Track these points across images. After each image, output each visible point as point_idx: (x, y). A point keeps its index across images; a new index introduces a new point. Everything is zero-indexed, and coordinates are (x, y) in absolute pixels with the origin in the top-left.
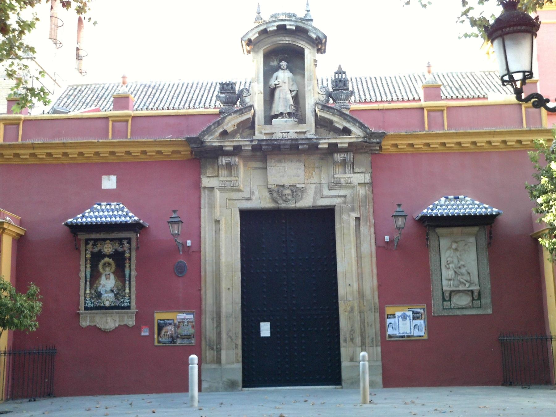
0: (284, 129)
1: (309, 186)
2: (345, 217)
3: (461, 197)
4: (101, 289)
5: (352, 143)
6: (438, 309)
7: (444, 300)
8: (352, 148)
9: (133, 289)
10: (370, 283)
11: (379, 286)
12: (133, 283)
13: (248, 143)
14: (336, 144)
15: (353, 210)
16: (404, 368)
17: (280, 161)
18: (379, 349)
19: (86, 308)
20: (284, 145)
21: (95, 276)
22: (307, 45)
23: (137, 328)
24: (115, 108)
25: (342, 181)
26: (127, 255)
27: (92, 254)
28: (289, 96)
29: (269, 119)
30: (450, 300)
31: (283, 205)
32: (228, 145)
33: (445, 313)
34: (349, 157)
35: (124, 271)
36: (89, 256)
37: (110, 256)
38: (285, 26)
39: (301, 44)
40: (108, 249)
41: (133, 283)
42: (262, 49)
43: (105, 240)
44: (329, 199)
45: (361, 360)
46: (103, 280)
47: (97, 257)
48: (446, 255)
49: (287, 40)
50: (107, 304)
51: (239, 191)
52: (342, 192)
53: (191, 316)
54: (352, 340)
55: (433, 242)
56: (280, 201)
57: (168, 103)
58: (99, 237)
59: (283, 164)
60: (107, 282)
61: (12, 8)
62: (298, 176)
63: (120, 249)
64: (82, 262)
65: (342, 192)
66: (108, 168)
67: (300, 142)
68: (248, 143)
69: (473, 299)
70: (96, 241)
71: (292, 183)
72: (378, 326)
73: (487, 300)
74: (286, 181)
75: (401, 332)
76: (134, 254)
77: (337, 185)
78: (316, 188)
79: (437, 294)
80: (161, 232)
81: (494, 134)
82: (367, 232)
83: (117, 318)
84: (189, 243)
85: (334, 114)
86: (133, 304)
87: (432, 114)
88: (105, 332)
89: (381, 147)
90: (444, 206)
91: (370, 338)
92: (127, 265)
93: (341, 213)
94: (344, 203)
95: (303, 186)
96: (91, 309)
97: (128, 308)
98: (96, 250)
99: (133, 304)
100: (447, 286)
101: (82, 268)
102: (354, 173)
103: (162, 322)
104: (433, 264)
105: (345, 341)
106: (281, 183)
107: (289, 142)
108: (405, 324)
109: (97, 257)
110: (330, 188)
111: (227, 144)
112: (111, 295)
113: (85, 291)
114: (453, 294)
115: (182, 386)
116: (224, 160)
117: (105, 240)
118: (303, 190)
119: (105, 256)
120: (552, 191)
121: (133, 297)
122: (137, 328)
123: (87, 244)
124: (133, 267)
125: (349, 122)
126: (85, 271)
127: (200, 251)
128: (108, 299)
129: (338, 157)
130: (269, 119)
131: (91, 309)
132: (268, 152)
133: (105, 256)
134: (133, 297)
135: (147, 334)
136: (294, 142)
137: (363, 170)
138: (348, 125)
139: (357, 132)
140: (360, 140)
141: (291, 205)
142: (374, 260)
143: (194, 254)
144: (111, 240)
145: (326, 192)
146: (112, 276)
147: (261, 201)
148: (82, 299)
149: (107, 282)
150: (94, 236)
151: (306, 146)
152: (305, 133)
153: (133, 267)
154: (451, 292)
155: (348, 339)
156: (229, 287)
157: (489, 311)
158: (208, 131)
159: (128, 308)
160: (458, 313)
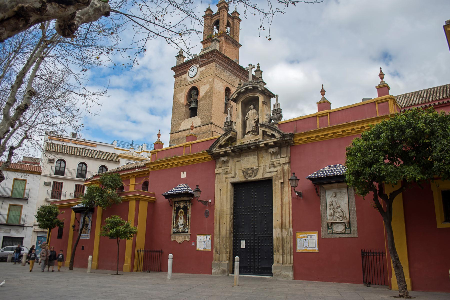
0: (249, 139)
1: (264, 167)
2: (277, 183)
3: (338, 165)
4: (179, 224)
5: (240, 267)
6: (325, 234)
7: (328, 228)
8: (276, 144)
9: (190, 224)
10: (288, 219)
11: (293, 220)
12: (190, 221)
13: (229, 149)
14: (268, 143)
15: (280, 178)
16: (307, 268)
17: (246, 156)
18: (292, 257)
19: (173, 233)
20: (245, 147)
21: (177, 217)
22: (260, 95)
23: (190, 242)
24: (55, 174)
25: (275, 163)
26: (188, 208)
27: (177, 208)
28: (253, 122)
29: (244, 134)
30: (332, 229)
31: (249, 179)
32: (222, 151)
33: (329, 236)
34: (275, 149)
35: (187, 215)
36: (175, 209)
37: (182, 209)
38: (248, 87)
39: (257, 95)
40: (182, 206)
41: (190, 221)
42: (162, 149)
43: (181, 201)
44: (219, 198)
45: (281, 262)
46: (180, 220)
47: (178, 209)
48: (329, 199)
49: (251, 94)
50: (180, 230)
51: (230, 173)
52: (275, 169)
53: (171, 255)
54: (278, 251)
55: (322, 195)
56: (247, 177)
57: (417, 101)
58: (68, 250)
59: (248, 158)
60: (181, 221)
61: (278, 112)
62: (254, 163)
63: (186, 205)
64: (173, 210)
65: (275, 169)
66: (182, 168)
67: (251, 145)
68: (229, 149)
69: (346, 228)
70: (178, 202)
71: (252, 167)
72: (292, 244)
73: (354, 228)
74: (250, 166)
75: (222, 125)
76: (190, 207)
77: (272, 166)
78: (264, 168)
79: (324, 225)
80: (201, 196)
81: (355, 123)
82: (287, 189)
83: (183, 236)
84: (210, 201)
85: (266, 128)
86: (189, 231)
87: (321, 118)
88: (180, 244)
89: (294, 142)
90: (327, 170)
91: (288, 250)
92: (98, 148)
93: (275, 181)
94: (277, 175)
95: (257, 168)
96: (175, 233)
97: (187, 232)
98: (178, 206)
99: (189, 231)
100: (330, 219)
101: (173, 215)
102: (281, 158)
103: (402, 276)
104: (322, 209)
105: (275, 252)
106: (247, 168)
107: (246, 146)
108: (309, 242)
109: (178, 209)
110: (270, 167)
111: (221, 151)
112: (182, 226)
113: (173, 224)
114: (333, 225)
115: (162, 269)
116: (222, 159)
117: (181, 201)
118: (257, 170)
119: (181, 208)
120: (449, 98)
121: (189, 227)
122: (190, 242)
123: (175, 203)
124: (190, 213)
125: (273, 130)
126: (173, 216)
127: (214, 205)
128: (181, 228)
129: (271, 150)
130: (244, 134)
131: (175, 233)
132: (242, 151)
133: (181, 208)
134: (189, 227)
135: (88, 238)
136: (248, 145)
137: (285, 156)
138: (273, 132)
139: (277, 135)
140: (278, 139)
141: (252, 179)
142: (291, 205)
143: (212, 206)
144: (183, 201)
145: (268, 170)
146: (183, 218)
147: (240, 178)
148: (172, 228)
149: (181, 221)
150: (177, 200)
151: (254, 147)
152: (258, 140)
153: (190, 213)
154: (332, 224)
155: (277, 251)
156: (81, 69)
157: (356, 236)
158: (213, 146)
159: (187, 232)
160: (338, 236)
